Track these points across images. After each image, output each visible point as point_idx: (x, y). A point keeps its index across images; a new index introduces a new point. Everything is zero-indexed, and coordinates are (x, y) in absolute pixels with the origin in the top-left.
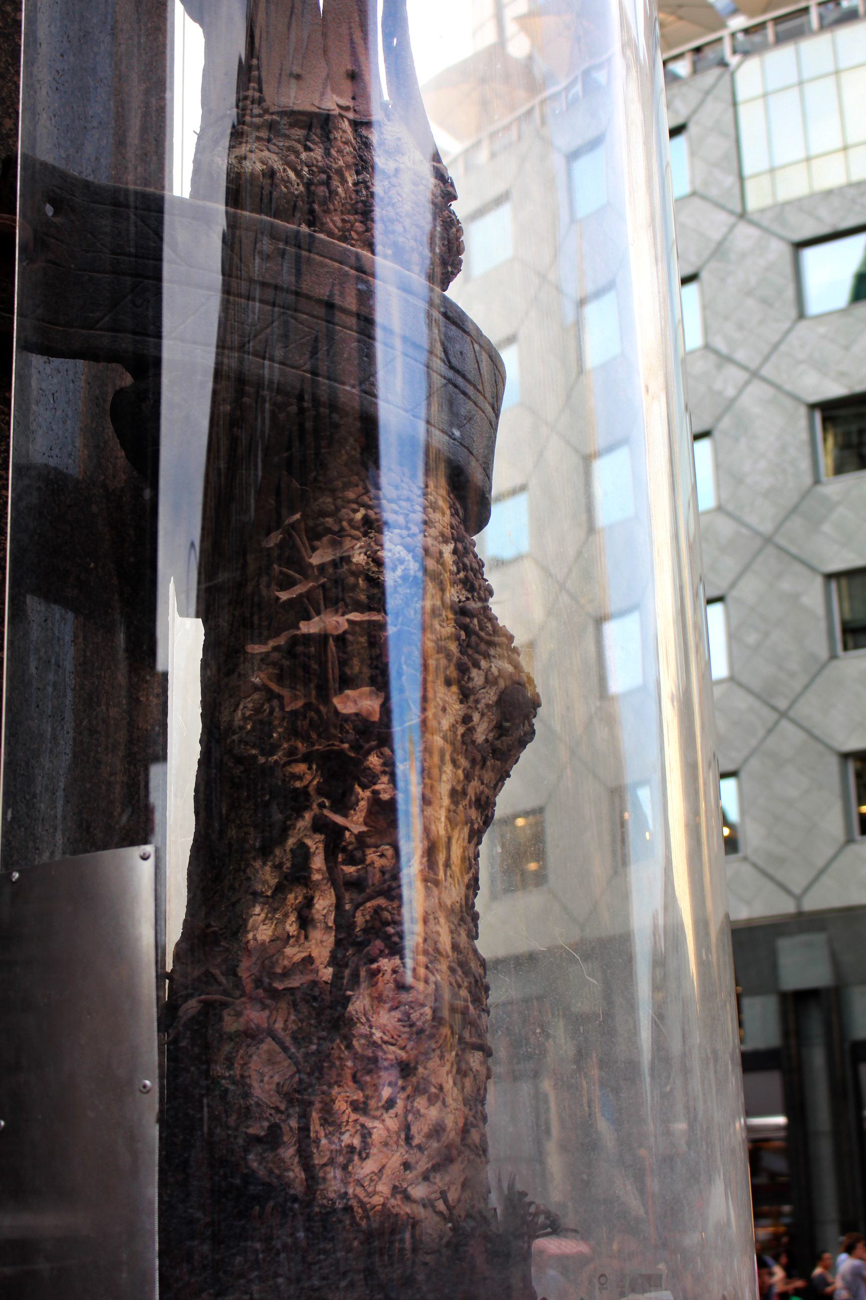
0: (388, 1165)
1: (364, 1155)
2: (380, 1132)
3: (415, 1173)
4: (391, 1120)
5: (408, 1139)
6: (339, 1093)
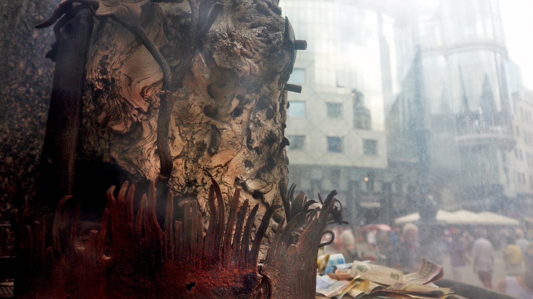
0: (233, 161)
3: (252, 170)
5: (249, 141)
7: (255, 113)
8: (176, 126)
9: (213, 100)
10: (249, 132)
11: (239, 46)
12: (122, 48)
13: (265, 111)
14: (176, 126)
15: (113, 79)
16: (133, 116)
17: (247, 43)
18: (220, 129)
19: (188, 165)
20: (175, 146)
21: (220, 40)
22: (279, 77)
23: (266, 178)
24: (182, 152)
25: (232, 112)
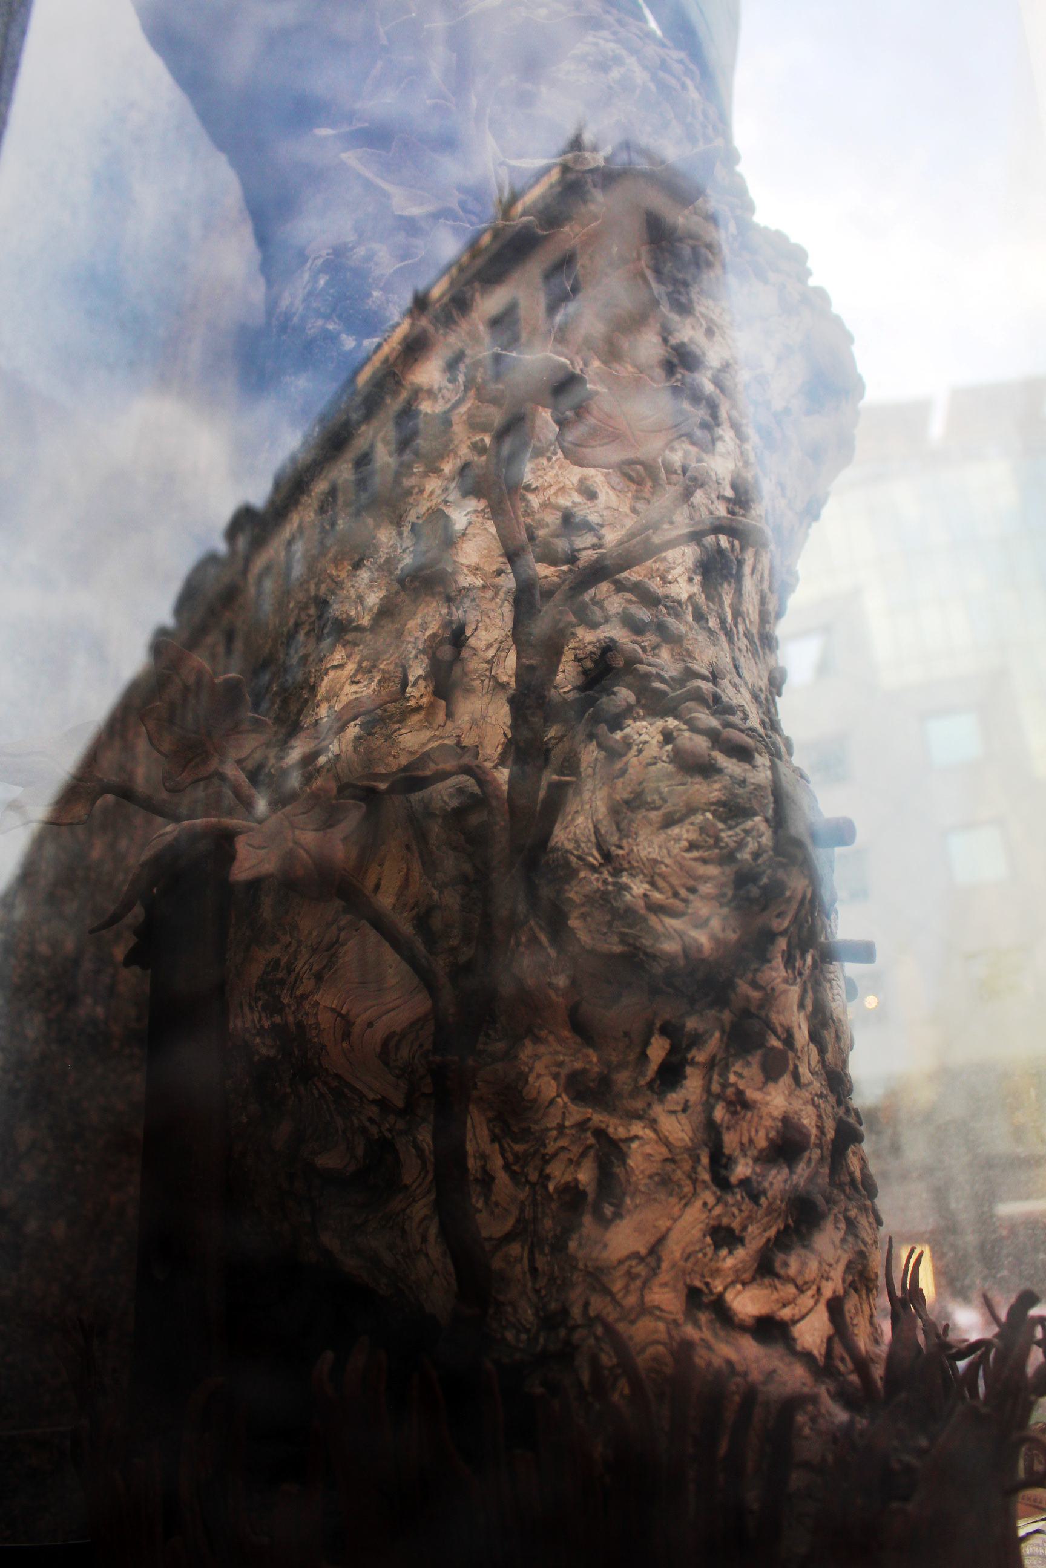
0: (674, 1236)
1: (608, 1210)
2: (648, 1149)
3: (740, 1253)
4: (673, 1118)
5: (720, 1163)
6: (537, 1057)
7: (726, 1068)
8: (492, 1141)
9: (590, 1051)
10: (712, 1133)
11: (639, 887)
12: (315, 933)
13: (756, 1059)
14: (492, 1141)
15: (300, 1025)
16: (367, 1124)
17: (660, 875)
18: (621, 1140)
19: (541, 1262)
20: (497, 1204)
21: (582, 874)
22: (782, 943)
23: (792, 1271)
24: (518, 1221)
25: (652, 1081)
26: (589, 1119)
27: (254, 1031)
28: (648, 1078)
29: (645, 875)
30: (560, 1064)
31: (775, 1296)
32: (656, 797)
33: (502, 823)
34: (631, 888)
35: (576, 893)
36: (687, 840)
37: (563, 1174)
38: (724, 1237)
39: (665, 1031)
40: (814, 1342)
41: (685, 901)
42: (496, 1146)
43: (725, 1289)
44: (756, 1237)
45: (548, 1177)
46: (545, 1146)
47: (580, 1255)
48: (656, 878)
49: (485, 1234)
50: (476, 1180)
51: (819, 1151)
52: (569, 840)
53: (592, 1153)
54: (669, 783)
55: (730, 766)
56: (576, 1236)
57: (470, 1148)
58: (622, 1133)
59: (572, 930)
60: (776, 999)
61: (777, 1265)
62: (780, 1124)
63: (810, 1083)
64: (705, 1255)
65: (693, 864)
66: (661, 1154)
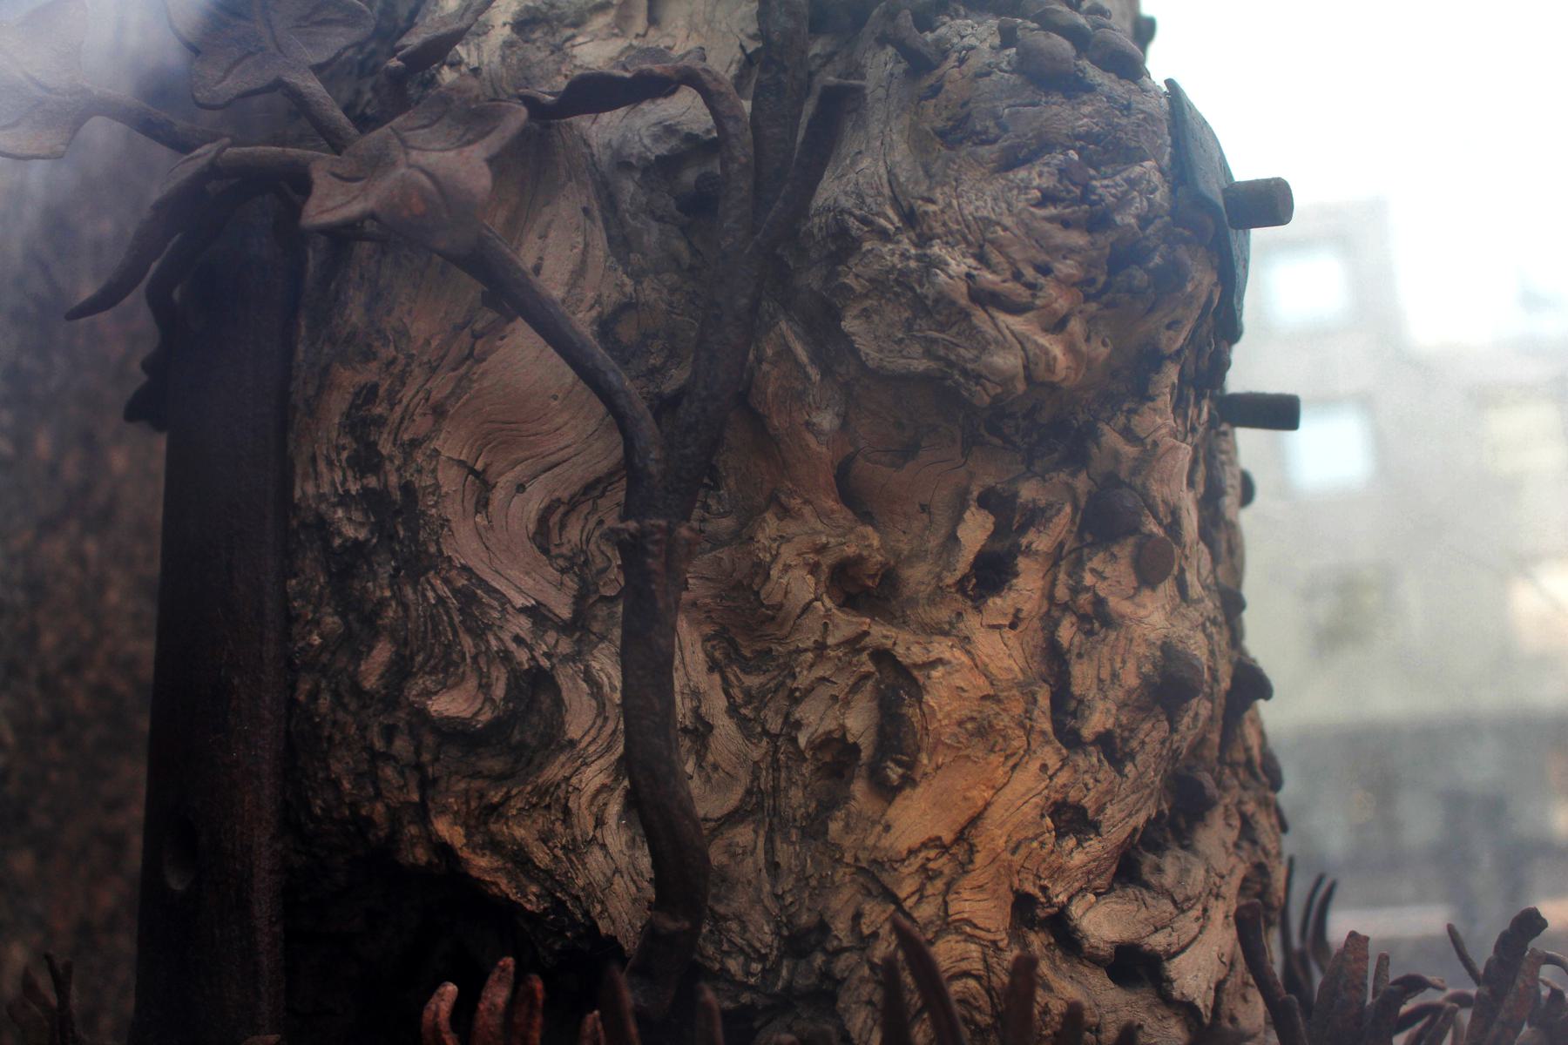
0: (995, 813)
1: (894, 773)
3: (1094, 845)
4: (996, 635)
5: (1065, 707)
6: (783, 539)
7: (1079, 564)
8: (711, 670)
10: (1055, 660)
11: (958, 263)
12: (434, 343)
13: (1125, 550)
15: (408, 489)
16: (513, 646)
17: (992, 242)
18: (915, 665)
19: (784, 853)
20: (716, 767)
21: (867, 246)
22: (1171, 374)
23: (1168, 879)
24: (749, 792)
26: (866, 633)
27: (334, 500)
28: (958, 575)
29: (969, 244)
30: (822, 549)
31: (1143, 914)
32: (990, 123)
33: (743, 160)
34: (947, 264)
35: (857, 276)
36: (1039, 188)
37: (822, 719)
38: (1071, 819)
39: (984, 502)
40: (1198, 986)
41: (1031, 286)
42: (716, 677)
43: (1070, 899)
44: (1122, 819)
45: (798, 725)
46: (794, 677)
47: (848, 842)
48: (988, 248)
49: (701, 812)
50: (685, 730)
51: (1209, 705)
52: (846, 193)
53: (869, 685)
54: (1011, 102)
55: (1106, 82)
56: (840, 814)
57: (678, 682)
58: (917, 654)
59: (846, 336)
60: (1158, 460)
61: (1146, 870)
62: (1158, 653)
63: (1200, 600)
64: (1042, 844)
65: (1047, 226)
66: (979, 688)
